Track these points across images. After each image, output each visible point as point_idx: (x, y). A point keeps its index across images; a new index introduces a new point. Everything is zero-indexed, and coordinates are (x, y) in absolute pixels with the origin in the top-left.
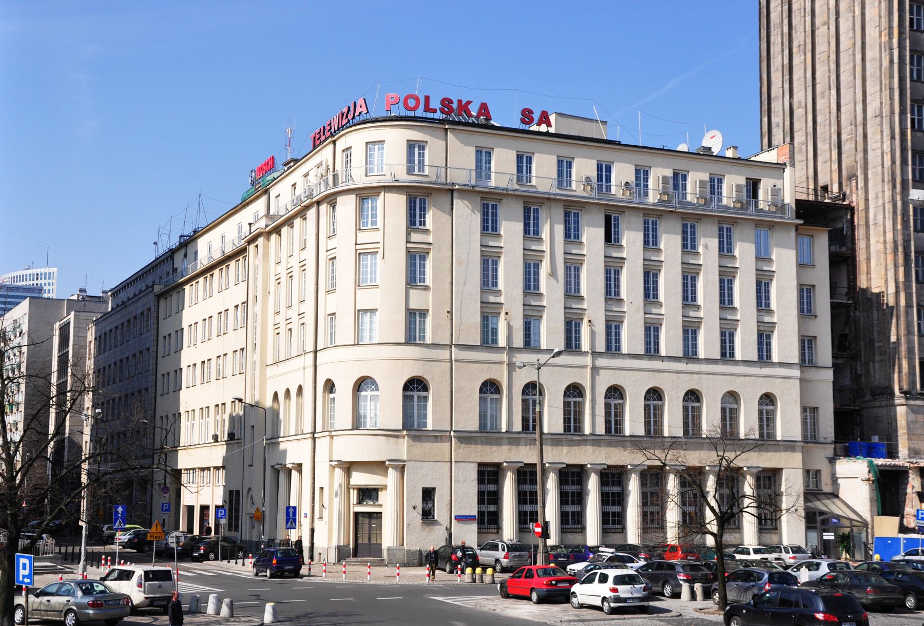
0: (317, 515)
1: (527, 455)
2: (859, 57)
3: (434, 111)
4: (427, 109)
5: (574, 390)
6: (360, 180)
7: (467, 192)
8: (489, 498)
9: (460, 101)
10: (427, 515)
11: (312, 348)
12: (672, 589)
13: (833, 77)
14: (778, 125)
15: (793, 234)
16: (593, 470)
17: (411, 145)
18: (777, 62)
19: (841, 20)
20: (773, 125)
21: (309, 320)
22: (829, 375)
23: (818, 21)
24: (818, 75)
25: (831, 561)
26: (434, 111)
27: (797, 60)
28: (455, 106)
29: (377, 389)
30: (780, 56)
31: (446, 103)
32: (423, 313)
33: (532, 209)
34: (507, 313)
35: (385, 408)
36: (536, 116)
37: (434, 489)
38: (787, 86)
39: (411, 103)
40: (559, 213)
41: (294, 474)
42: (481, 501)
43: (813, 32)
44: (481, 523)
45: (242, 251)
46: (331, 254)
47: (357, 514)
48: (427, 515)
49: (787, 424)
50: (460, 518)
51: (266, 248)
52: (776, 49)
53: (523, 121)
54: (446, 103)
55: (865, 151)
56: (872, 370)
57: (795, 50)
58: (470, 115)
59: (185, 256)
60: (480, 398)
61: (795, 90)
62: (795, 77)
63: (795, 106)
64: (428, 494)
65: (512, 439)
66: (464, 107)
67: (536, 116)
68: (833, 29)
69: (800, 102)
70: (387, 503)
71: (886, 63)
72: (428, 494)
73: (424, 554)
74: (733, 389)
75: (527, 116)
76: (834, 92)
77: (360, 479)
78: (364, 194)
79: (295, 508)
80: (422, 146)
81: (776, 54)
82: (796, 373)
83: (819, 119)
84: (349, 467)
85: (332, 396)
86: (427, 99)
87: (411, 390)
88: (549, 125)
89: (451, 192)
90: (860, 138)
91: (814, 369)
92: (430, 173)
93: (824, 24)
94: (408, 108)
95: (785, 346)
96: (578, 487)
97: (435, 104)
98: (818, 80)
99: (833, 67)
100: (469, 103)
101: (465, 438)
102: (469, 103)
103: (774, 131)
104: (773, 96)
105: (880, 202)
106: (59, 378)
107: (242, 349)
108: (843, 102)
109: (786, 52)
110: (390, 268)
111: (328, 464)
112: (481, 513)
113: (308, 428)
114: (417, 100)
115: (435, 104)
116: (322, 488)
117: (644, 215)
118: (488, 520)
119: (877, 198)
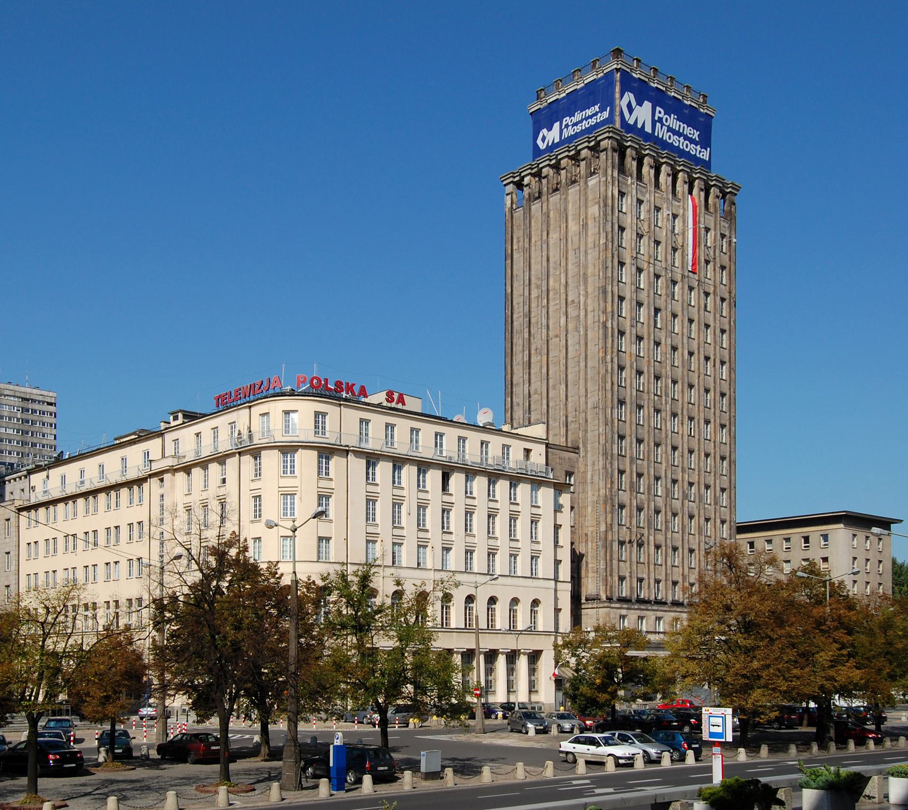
2: (582, 364)
5: (515, 601)
6: (279, 437)
7: (359, 453)
12: (314, 771)
13: (563, 376)
14: (518, 405)
16: (457, 653)
17: (317, 414)
18: (518, 358)
20: (515, 404)
24: (550, 372)
28: (344, 386)
30: (521, 355)
32: (328, 539)
38: (526, 377)
40: (439, 474)
45: (139, 482)
52: (518, 348)
53: (387, 400)
55: (586, 431)
57: (533, 352)
59: (48, 477)
61: (532, 381)
62: (532, 371)
63: (532, 392)
69: (536, 390)
71: (602, 371)
76: (563, 386)
78: (288, 450)
80: (324, 415)
83: (551, 404)
86: (326, 380)
88: (404, 404)
92: (330, 438)
93: (556, 336)
95: (545, 567)
98: (550, 376)
99: (563, 368)
100: (354, 385)
102: (354, 385)
103: (515, 408)
104: (514, 383)
105: (596, 468)
108: (569, 395)
109: (527, 352)
114: (319, 380)
117: (393, 461)
119: (594, 464)
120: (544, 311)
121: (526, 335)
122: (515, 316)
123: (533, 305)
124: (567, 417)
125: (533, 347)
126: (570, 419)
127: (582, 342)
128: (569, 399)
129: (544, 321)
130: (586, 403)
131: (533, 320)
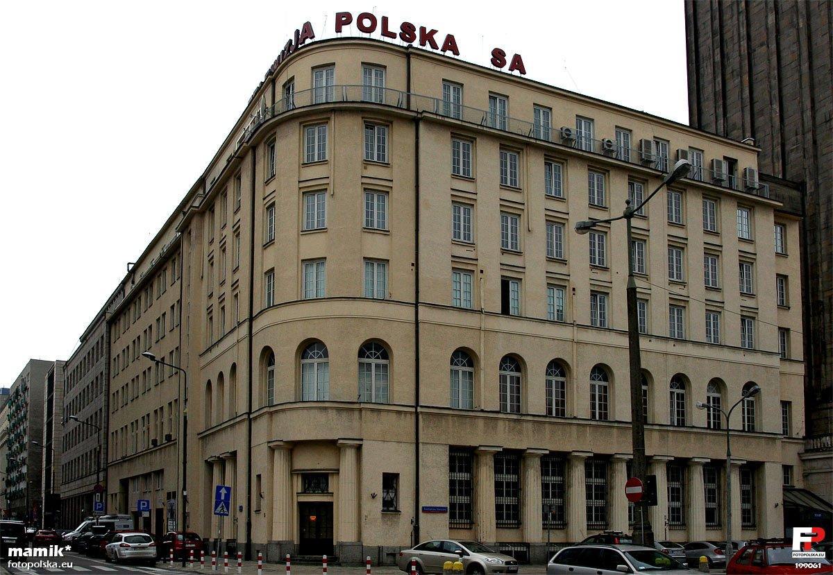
0: (254, 507)
1: (504, 438)
2: (805, 67)
3: (393, 36)
4: (385, 32)
8: (463, 489)
9: (423, 29)
10: (390, 506)
11: (247, 316)
15: (772, 218)
19: (782, 37)
21: (243, 275)
22: (800, 369)
23: (755, 43)
24: (755, 95)
25: (727, 564)
26: (393, 36)
27: (732, 84)
29: (326, 355)
31: (407, 29)
33: (512, 145)
34: (482, 272)
35: (339, 376)
36: (509, 59)
37: (399, 474)
39: (367, 23)
41: (229, 468)
42: (452, 492)
43: (749, 54)
44: (452, 516)
46: (269, 201)
47: (300, 504)
48: (390, 506)
49: (770, 420)
50: (427, 510)
51: (201, 228)
54: (407, 29)
55: (815, 157)
56: (823, 372)
57: (728, 76)
58: (434, 46)
60: (361, 365)
62: (729, 102)
64: (390, 481)
65: (491, 418)
66: (428, 36)
67: (509, 59)
68: (773, 47)
70: (343, 494)
72: (390, 481)
73: (385, 551)
74: (718, 376)
75: (498, 56)
76: (776, 107)
77: (307, 462)
79: (228, 489)
81: (706, 84)
82: (775, 361)
84: (293, 447)
85: (270, 369)
86: (385, 20)
87: (368, 357)
89: (416, 121)
90: (809, 146)
91: (787, 363)
94: (361, 28)
95: (767, 337)
96: (559, 478)
97: (394, 27)
99: (775, 82)
100: (434, 32)
101: (437, 414)
102: (434, 32)
106: (47, 442)
107: (176, 401)
109: (719, 79)
110: (346, 204)
111: (265, 447)
112: (452, 505)
113: (242, 408)
115: (394, 27)
116: (259, 476)
118: (462, 513)
120: (743, 18)
121: (718, 58)
122: (701, 40)
123: (726, 17)
124: (783, 146)
125: (729, 70)
126: (788, 148)
127: (803, 37)
128: (786, 121)
129: (743, 31)
130: (814, 118)
131: (727, 36)
